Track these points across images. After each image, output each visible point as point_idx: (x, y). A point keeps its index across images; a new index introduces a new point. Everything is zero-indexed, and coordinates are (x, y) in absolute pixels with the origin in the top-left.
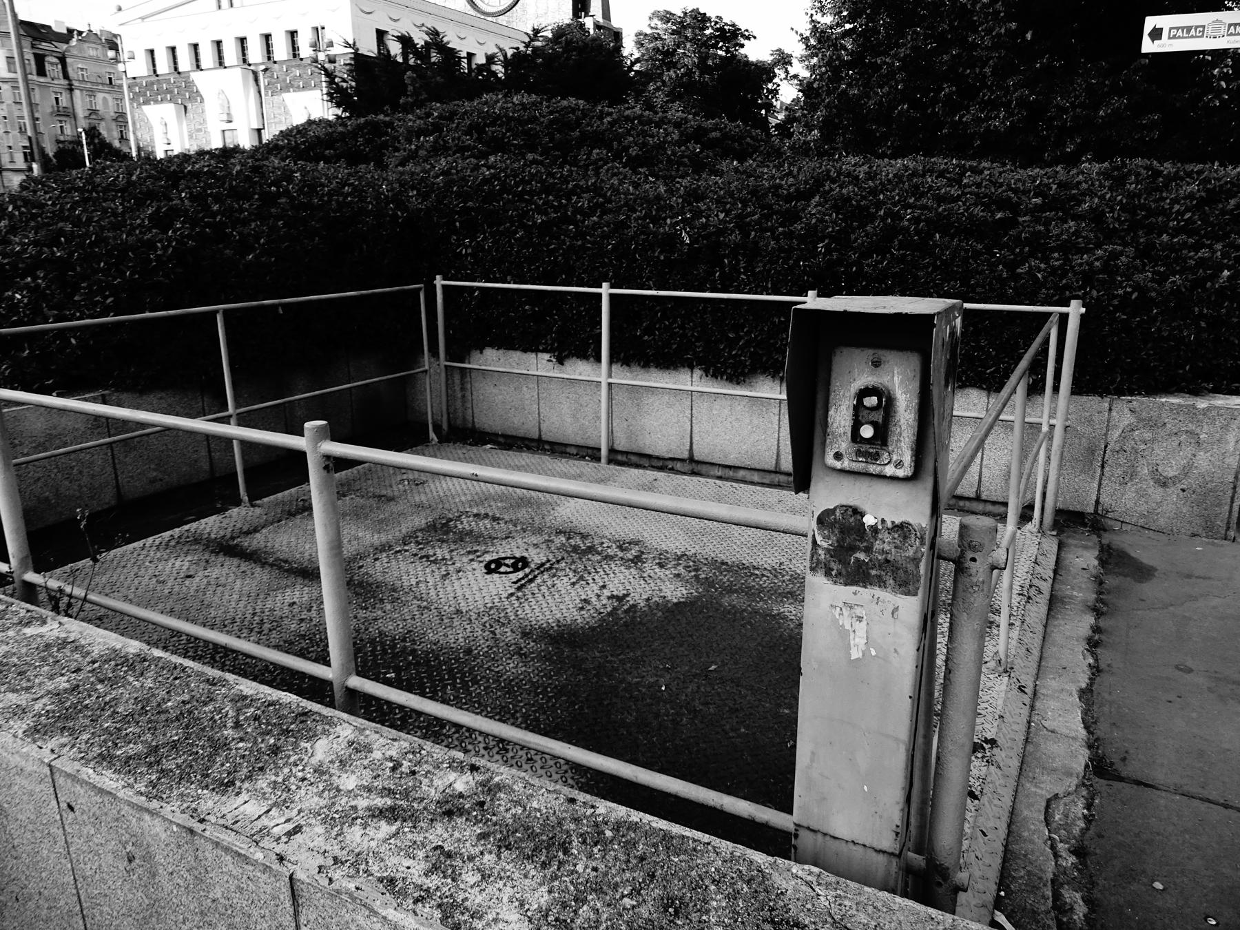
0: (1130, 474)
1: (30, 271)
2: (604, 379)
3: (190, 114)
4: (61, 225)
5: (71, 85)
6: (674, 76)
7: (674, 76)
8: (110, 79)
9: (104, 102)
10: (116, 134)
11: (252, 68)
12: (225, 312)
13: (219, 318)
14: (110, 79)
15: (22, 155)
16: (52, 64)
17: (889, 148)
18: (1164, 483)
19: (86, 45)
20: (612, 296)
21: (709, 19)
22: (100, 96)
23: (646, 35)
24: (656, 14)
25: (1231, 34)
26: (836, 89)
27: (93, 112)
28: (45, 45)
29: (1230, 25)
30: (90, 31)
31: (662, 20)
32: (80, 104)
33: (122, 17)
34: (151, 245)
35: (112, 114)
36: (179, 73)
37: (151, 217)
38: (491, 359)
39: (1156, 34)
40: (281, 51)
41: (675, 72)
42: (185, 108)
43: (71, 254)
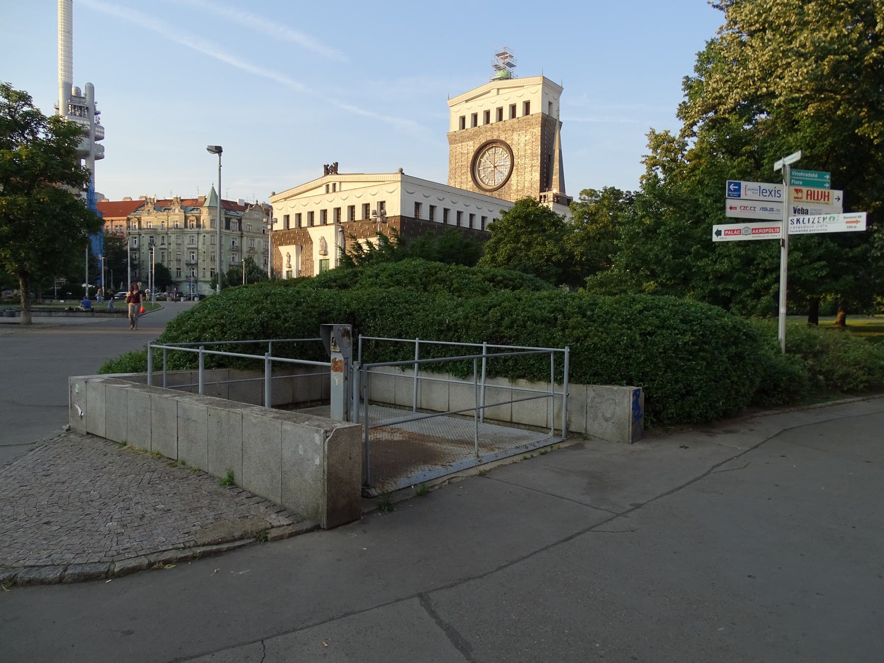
0: (595, 417)
1: (213, 327)
2: (415, 376)
3: (304, 251)
4: (225, 312)
5: (242, 234)
6: (595, 228)
7: (595, 228)
8: (264, 230)
9: (258, 243)
10: (262, 261)
11: (342, 225)
12: (272, 342)
13: (270, 344)
14: (264, 230)
15: (210, 273)
16: (234, 223)
17: (664, 279)
18: (606, 420)
19: (254, 212)
20: (419, 343)
21: (622, 193)
22: (257, 240)
23: (577, 204)
24: (584, 192)
25: (754, 233)
26: (631, 247)
27: (252, 249)
28: (232, 213)
29: (753, 229)
30: (257, 204)
31: (588, 195)
32: (245, 244)
33: (275, 198)
34: (253, 320)
35: (262, 250)
36: (301, 228)
37: (255, 310)
38: (380, 370)
39: (719, 233)
40: (359, 215)
41: (596, 226)
42: (302, 247)
43: (226, 322)
